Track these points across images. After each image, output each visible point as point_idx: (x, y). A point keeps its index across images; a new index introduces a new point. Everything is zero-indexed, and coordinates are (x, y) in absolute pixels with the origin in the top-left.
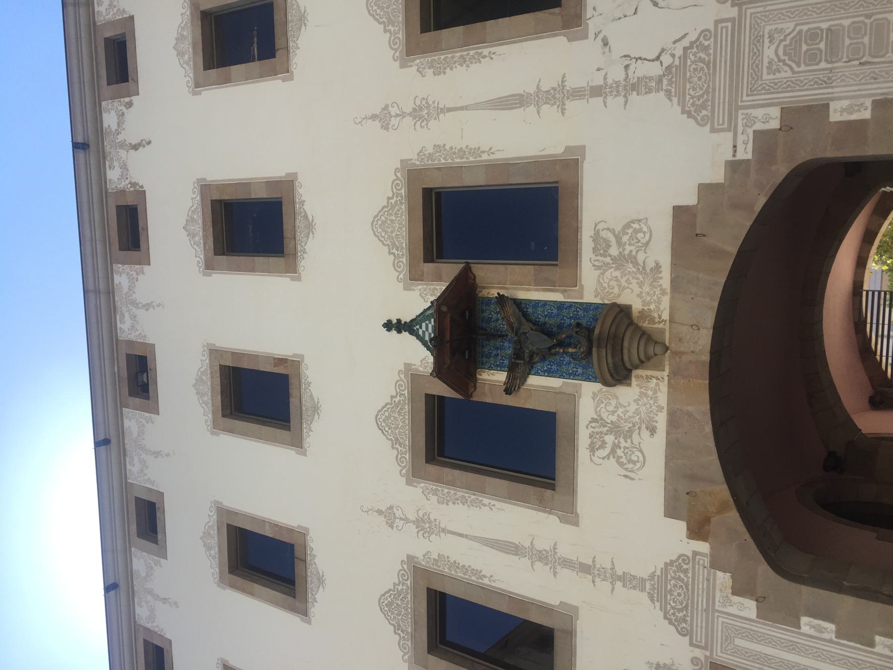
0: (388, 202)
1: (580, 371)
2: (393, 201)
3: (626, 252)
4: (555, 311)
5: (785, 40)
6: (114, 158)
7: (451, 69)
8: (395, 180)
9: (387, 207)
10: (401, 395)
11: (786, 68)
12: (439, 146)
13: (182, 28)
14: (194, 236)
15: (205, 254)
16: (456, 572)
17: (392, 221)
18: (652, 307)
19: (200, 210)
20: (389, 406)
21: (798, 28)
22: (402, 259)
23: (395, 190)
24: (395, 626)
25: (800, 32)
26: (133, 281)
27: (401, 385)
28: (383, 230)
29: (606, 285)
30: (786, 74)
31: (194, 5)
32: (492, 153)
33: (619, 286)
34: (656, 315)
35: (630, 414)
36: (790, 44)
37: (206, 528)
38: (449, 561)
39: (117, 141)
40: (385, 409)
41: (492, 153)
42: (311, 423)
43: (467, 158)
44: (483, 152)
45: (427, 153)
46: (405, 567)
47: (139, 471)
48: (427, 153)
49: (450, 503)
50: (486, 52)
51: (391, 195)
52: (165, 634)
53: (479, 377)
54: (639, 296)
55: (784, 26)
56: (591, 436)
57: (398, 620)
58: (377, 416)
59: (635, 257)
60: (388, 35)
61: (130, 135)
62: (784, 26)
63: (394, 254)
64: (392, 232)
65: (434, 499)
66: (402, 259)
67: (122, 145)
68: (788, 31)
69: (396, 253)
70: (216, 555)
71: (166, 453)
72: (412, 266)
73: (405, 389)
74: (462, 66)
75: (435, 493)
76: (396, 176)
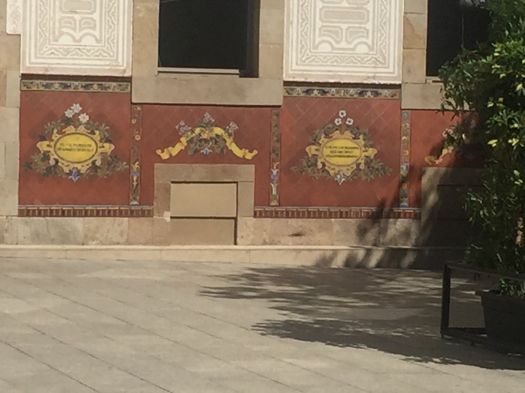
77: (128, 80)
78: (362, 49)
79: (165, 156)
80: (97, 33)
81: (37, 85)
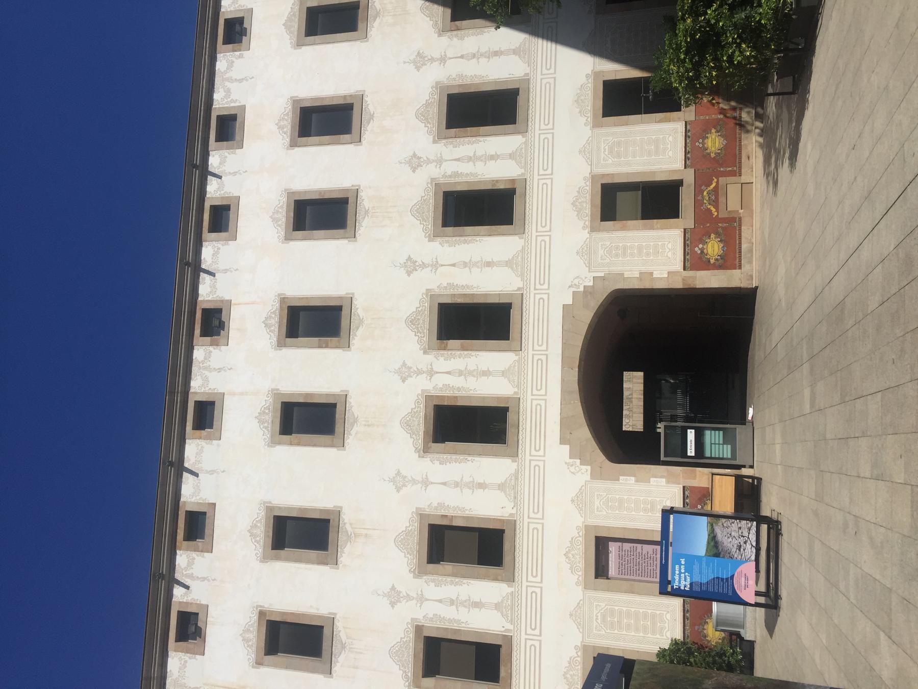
0: (412, 411)
2: (420, 309)
5: (603, 499)
6: (198, 374)
7: (463, 145)
8: (412, 517)
9: (411, 413)
11: (608, 259)
12: (446, 385)
13: (271, 313)
14: (283, 128)
15: (291, 139)
16: (458, 290)
17: (418, 319)
19: (278, 313)
20: (398, 644)
21: (607, 607)
23: (406, 634)
24: (420, 220)
25: (607, 609)
26: (231, 64)
27: (408, 631)
28: (418, 212)
30: (607, 261)
31: (301, 4)
32: (468, 624)
36: (604, 612)
37: (262, 409)
38: (445, 506)
39: (225, 77)
40: (402, 534)
41: (468, 624)
42: (344, 548)
43: (453, 624)
44: (471, 390)
45: (433, 506)
46: (409, 626)
47: (183, 594)
48: (433, 506)
49: (443, 586)
50: (469, 458)
51: (403, 636)
52: (218, 390)
55: (603, 494)
57: (408, 549)
58: (401, 421)
60: (417, 337)
61: (234, 74)
62: (603, 494)
64: (423, 213)
65: (446, 245)
67: (231, 80)
68: (603, 607)
69: (420, 335)
70: (276, 330)
71: (213, 579)
72: (420, 565)
73: (416, 522)
74: (451, 585)
75: (433, 581)
76: (427, 185)
77: (684, 487)
78: (668, 616)
79: (716, 214)
80: (665, 613)
81: (688, 264)
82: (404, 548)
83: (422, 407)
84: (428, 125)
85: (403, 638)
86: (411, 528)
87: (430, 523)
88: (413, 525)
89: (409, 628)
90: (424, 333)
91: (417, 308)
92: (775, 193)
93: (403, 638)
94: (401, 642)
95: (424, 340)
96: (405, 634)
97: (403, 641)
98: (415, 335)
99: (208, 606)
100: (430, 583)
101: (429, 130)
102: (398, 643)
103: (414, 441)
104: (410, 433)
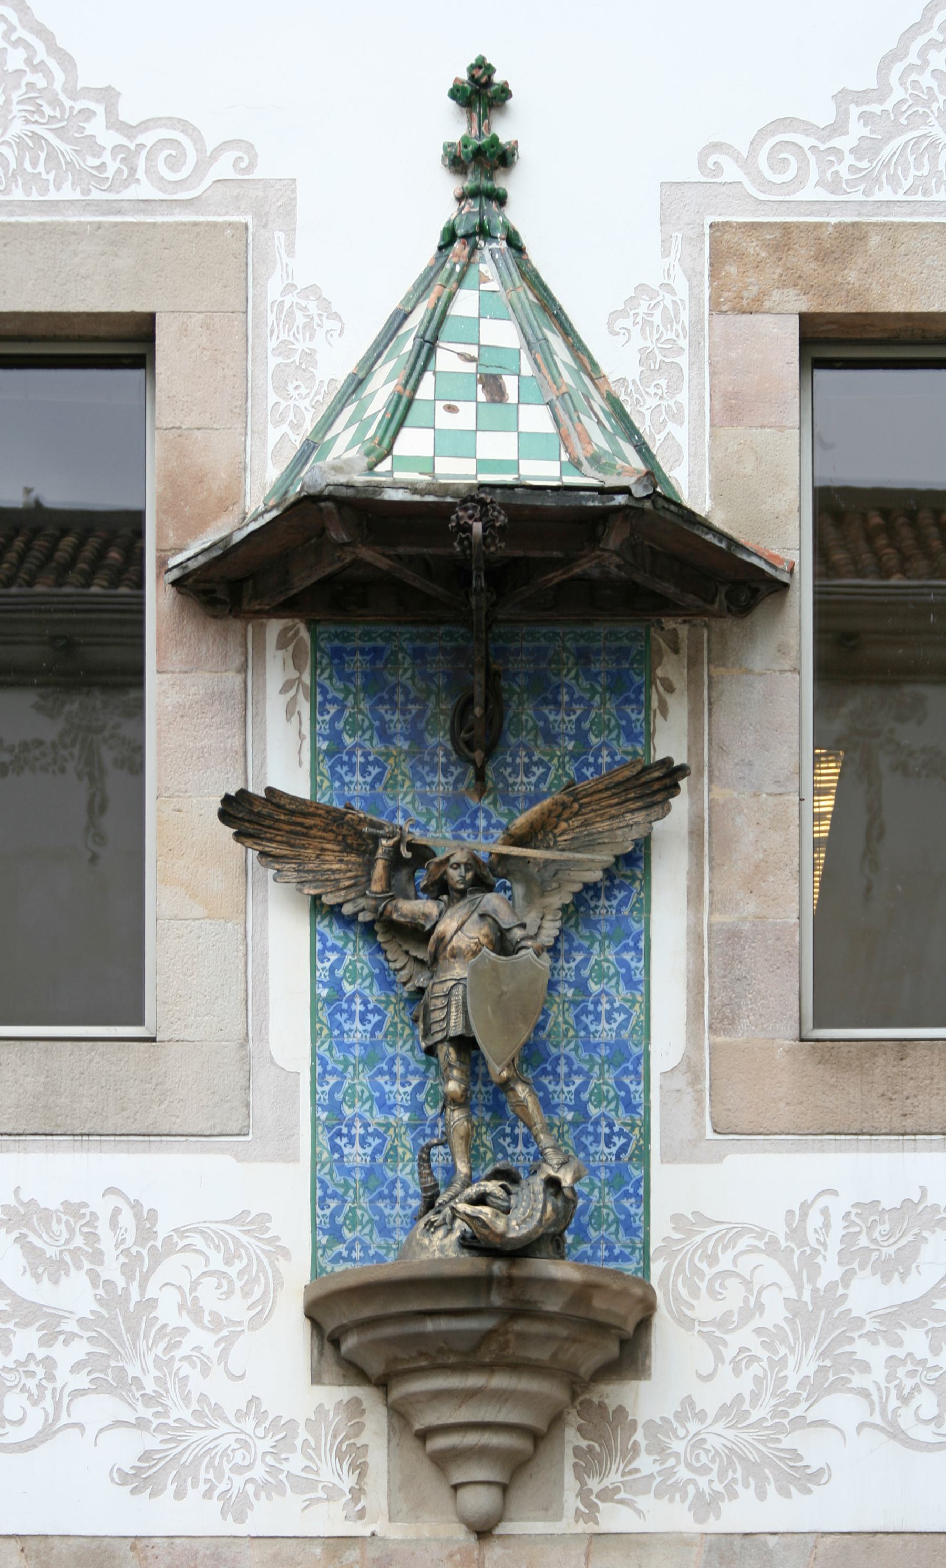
1: (356, 1155)
2: (96, 127)
3: (861, 1349)
4: (605, 1031)
10: (128, 157)
18: (645, 1463)
22: (814, 176)
23: (148, 138)
24: (882, 92)
29: (725, 1261)
33: (723, 1322)
34: (614, 1478)
35: (197, 1384)
40: (41, 54)
53: (274, 627)
54: (688, 1406)
56: (74, 1210)
59: (841, 1385)
63: (838, 127)
66: (814, 176)
69: (844, 143)
82: (926, 80)
83: (131, 193)
84: (857, 129)
85: (111, 111)
86: (109, 139)
87: (157, 315)
88: (128, 157)
89: (205, 162)
90: (870, 179)
91: (108, 96)
92: (452, 855)
93: (111, 111)
94: (74, 94)
95: (799, 181)
96: (145, 126)
97: (88, 114)
98: (844, 98)
99: (389, 1520)
100: (638, 341)
101: (806, 142)
102: (66, 60)
103: (807, 128)
104: (882, 92)
